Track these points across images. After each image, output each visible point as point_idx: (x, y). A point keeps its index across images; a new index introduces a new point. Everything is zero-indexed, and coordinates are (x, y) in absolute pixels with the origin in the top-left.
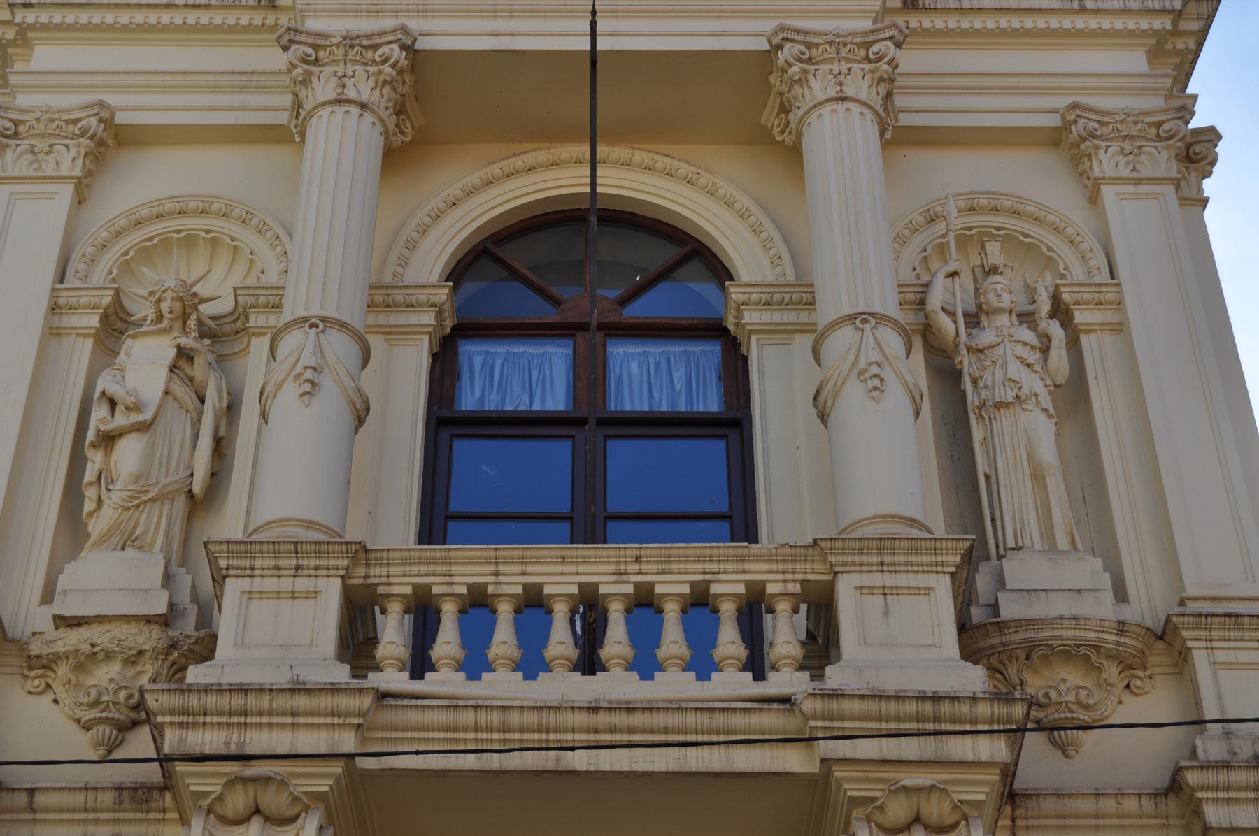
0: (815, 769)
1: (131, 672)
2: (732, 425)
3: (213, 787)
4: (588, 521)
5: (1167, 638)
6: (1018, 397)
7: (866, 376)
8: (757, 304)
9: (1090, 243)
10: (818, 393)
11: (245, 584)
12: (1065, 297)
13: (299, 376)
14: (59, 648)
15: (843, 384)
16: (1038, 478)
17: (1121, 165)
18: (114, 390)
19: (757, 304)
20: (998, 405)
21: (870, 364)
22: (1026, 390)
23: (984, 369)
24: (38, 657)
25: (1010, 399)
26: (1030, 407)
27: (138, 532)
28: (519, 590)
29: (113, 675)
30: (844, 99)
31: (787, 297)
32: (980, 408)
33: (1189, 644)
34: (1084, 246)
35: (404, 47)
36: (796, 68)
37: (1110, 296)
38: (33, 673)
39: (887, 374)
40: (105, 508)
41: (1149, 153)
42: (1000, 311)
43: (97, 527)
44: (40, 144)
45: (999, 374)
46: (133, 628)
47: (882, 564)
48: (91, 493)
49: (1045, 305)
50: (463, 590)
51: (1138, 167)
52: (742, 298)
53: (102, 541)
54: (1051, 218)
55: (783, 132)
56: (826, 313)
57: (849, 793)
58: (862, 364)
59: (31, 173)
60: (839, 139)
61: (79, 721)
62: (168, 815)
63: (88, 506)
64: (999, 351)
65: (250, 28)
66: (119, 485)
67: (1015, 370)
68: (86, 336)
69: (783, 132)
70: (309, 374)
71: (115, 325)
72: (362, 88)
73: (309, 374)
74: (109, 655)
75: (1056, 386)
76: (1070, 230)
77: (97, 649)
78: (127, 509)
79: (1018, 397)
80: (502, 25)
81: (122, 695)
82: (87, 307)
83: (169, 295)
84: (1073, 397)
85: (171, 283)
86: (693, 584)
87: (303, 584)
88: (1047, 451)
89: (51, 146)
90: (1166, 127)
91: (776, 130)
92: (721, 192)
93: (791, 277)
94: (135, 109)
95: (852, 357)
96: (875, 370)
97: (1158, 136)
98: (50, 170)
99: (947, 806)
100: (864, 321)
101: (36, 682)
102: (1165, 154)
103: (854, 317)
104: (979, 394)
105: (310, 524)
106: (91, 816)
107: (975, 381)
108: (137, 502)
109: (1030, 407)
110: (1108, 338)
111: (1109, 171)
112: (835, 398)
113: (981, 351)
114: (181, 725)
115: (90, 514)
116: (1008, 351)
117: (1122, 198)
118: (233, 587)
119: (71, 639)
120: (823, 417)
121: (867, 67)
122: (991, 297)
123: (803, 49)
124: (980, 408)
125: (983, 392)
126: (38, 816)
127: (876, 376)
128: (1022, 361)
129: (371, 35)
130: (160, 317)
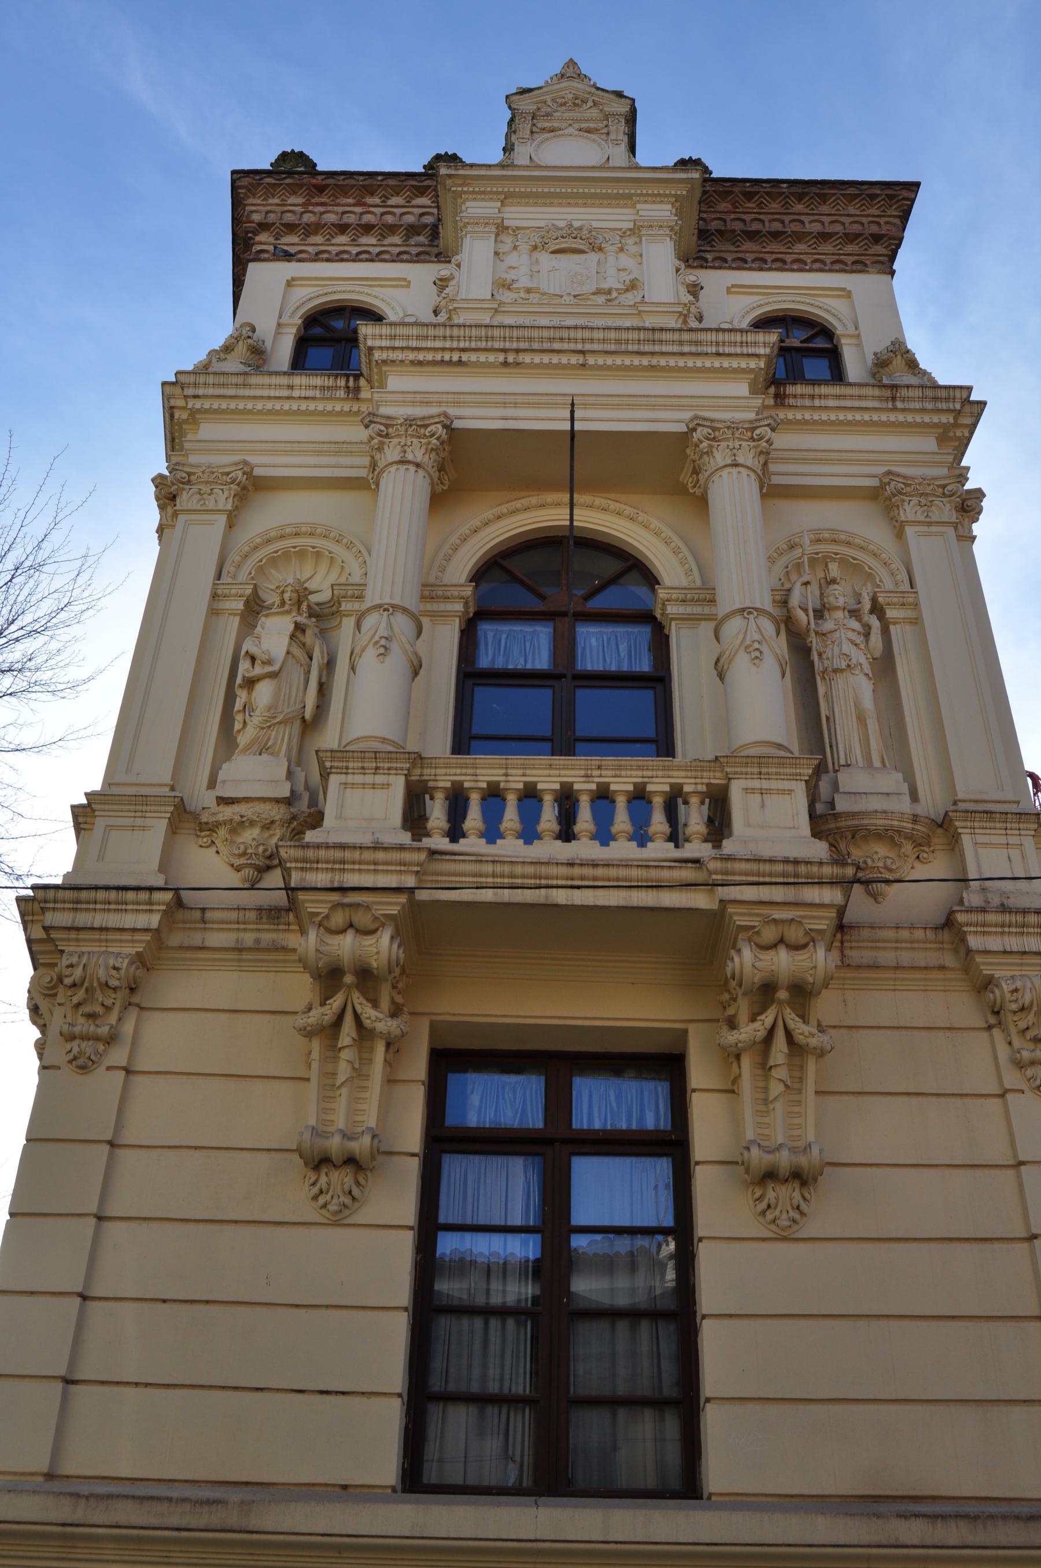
0: (715, 906)
1: (266, 834)
2: (658, 681)
3: (324, 910)
4: (564, 741)
5: (945, 826)
6: (849, 666)
7: (751, 649)
8: (677, 600)
9: (897, 564)
10: (718, 660)
11: (342, 778)
12: (880, 600)
13: (377, 643)
14: (220, 817)
15: (737, 651)
16: (861, 719)
17: (919, 513)
18: (254, 650)
19: (677, 600)
20: (836, 671)
21: (754, 641)
22: (854, 661)
23: (826, 646)
24: (207, 823)
25: (844, 667)
26: (857, 672)
27: (270, 744)
28: (521, 786)
29: (255, 836)
30: (737, 465)
31: (696, 596)
32: (823, 673)
33: (960, 830)
34: (893, 566)
35: (445, 426)
36: (705, 444)
37: (910, 600)
38: (203, 834)
39: (765, 648)
40: (248, 728)
41: (938, 506)
42: (837, 608)
43: (243, 740)
44: (206, 489)
45: (836, 650)
46: (267, 806)
47: (760, 773)
48: (239, 718)
49: (867, 605)
50: (484, 785)
51: (930, 514)
52: (666, 596)
53: (247, 749)
54: (871, 547)
55: (694, 487)
56: (724, 606)
57: (738, 923)
58: (748, 642)
59: (199, 507)
60: (733, 492)
61: (232, 865)
62: (291, 927)
63: (237, 726)
64: (837, 635)
65: (341, 413)
66: (258, 712)
67: (847, 648)
68: (235, 615)
69: (694, 487)
70: (383, 642)
71: (254, 608)
72: (417, 453)
73: (383, 642)
74: (252, 823)
75: (874, 659)
76: (884, 556)
77: (244, 819)
78: (263, 728)
79: (849, 666)
80: (510, 412)
81: (261, 849)
82: (236, 596)
83: (289, 589)
84: (884, 667)
85: (290, 581)
86: (635, 784)
87: (380, 779)
88: (868, 702)
89: (931, 501)
90: (949, 488)
91: (690, 485)
92: (652, 526)
93: (699, 583)
94: (266, 466)
95: (741, 636)
96: (756, 645)
97: (944, 493)
98: (211, 506)
99: (801, 933)
100: (749, 613)
101: (205, 840)
102: (948, 506)
103: (743, 610)
104: (823, 663)
105: (384, 740)
106: (242, 926)
107: (820, 655)
108: (269, 724)
109: (857, 672)
110: (908, 628)
111: (911, 517)
112: (730, 663)
113: (824, 635)
114: (302, 869)
115: (239, 731)
116: (843, 635)
117: (919, 534)
118: (334, 780)
119: (228, 812)
120: (721, 676)
121: (752, 444)
122: (832, 599)
123: (710, 431)
124: (823, 673)
125: (825, 662)
126: (207, 926)
127: (757, 649)
128: (852, 642)
129: (423, 418)
130: (283, 603)
